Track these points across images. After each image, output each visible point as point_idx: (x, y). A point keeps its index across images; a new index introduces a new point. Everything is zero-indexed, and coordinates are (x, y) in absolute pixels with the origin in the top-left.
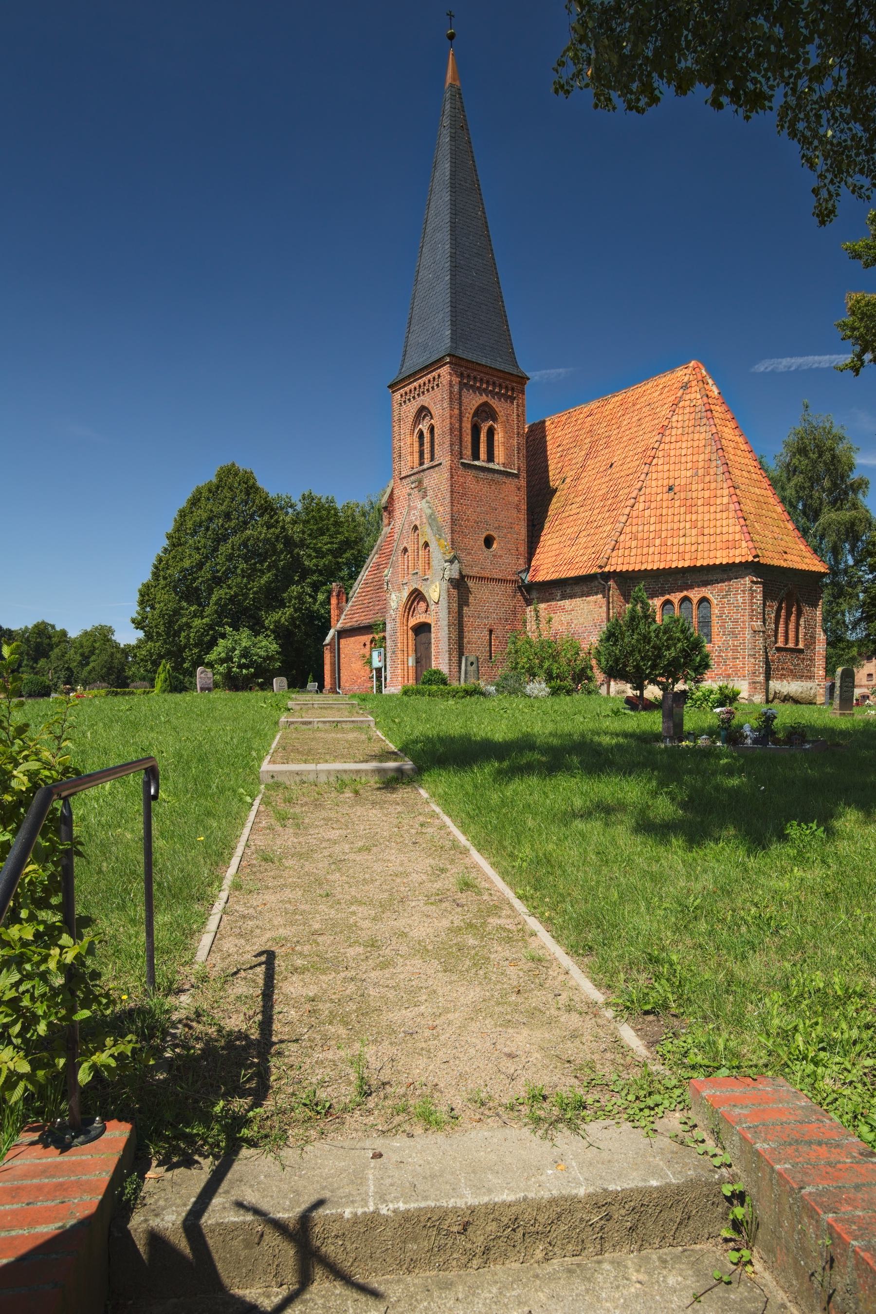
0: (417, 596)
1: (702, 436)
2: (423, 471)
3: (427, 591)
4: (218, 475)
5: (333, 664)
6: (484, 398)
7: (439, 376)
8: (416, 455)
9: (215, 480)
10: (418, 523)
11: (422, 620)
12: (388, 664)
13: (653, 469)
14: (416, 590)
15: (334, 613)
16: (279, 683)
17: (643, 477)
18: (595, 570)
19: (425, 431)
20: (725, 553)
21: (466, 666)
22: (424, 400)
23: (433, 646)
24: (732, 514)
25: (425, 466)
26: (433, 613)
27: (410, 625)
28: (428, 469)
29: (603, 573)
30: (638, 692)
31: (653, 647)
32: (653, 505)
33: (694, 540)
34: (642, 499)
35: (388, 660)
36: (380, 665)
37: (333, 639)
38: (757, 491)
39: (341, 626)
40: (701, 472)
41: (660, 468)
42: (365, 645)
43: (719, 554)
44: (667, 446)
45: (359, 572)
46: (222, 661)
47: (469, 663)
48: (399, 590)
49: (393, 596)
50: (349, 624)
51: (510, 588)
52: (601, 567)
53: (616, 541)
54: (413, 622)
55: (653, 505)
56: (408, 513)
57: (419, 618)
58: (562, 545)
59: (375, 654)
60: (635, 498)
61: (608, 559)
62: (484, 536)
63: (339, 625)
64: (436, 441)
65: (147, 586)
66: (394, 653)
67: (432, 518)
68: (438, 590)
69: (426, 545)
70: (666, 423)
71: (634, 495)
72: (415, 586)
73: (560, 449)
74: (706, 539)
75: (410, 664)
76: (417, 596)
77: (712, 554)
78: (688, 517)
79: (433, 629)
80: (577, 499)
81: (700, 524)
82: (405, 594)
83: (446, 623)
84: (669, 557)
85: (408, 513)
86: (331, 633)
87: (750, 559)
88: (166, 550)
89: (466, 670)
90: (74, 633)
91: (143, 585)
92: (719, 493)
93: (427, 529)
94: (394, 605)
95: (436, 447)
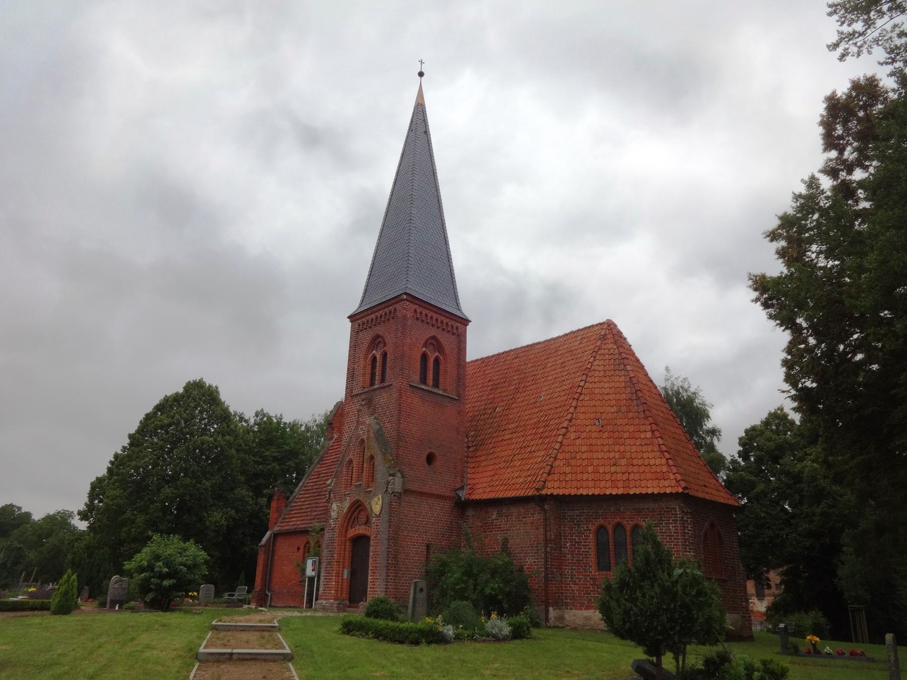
0: (358, 509)
1: (623, 378)
2: (374, 390)
3: (370, 503)
4: (185, 388)
5: (265, 566)
6: (433, 332)
7: (395, 310)
8: (368, 377)
9: (181, 391)
10: (365, 437)
11: (361, 532)
12: (322, 574)
13: (580, 403)
14: (358, 501)
15: (273, 516)
16: (207, 590)
17: (572, 410)
18: (531, 493)
19: (378, 357)
20: (655, 483)
21: (415, 593)
22: (380, 330)
23: (370, 560)
24: (656, 448)
25: (376, 387)
26: (373, 526)
27: (349, 536)
28: (379, 388)
29: (541, 496)
30: (654, 659)
31: (680, 606)
32: (584, 435)
33: (624, 469)
34: (572, 429)
35: (322, 570)
36: (313, 574)
37: (268, 541)
38: (672, 429)
39: (278, 529)
40: (624, 409)
41: (586, 403)
42: (298, 549)
43: (649, 484)
44: (591, 386)
45: (301, 479)
46: (141, 570)
47: (418, 590)
48: (341, 501)
49: (334, 506)
50: (286, 528)
51: (448, 505)
52: (538, 490)
53: (552, 466)
54: (352, 533)
55: (584, 435)
56: (356, 429)
57: (361, 530)
58: (497, 467)
59: (309, 563)
60: (566, 428)
61: (545, 482)
62: (427, 453)
63: (276, 529)
64: (388, 365)
65: (100, 480)
66: (329, 563)
67: (379, 434)
68: (380, 502)
69: (372, 458)
70: (589, 366)
71: (565, 425)
72: (357, 497)
73: (491, 383)
74: (635, 469)
75: (345, 576)
76: (358, 509)
77: (643, 483)
78: (617, 448)
79: (372, 543)
80: (511, 426)
81: (628, 455)
82: (347, 504)
83: (386, 537)
84: (603, 484)
85: (356, 429)
86: (268, 534)
87: (680, 490)
88: (124, 448)
89: (414, 598)
90: (37, 516)
91: (97, 478)
92: (642, 428)
93: (374, 444)
94: (334, 514)
95: (388, 370)
